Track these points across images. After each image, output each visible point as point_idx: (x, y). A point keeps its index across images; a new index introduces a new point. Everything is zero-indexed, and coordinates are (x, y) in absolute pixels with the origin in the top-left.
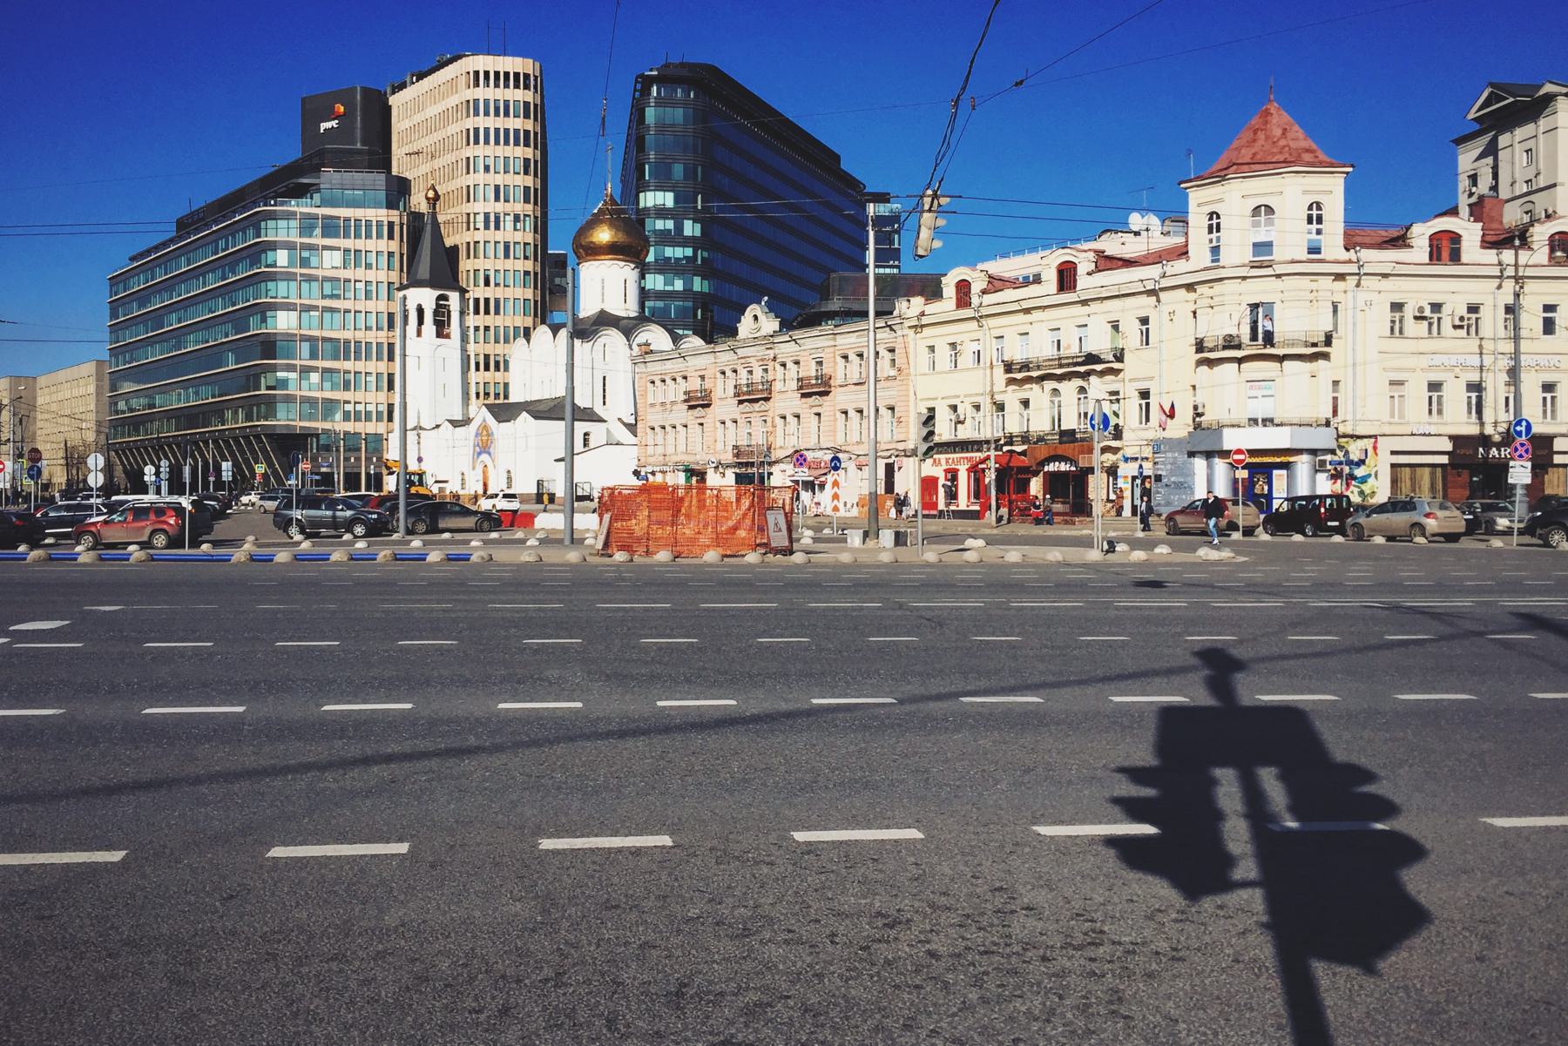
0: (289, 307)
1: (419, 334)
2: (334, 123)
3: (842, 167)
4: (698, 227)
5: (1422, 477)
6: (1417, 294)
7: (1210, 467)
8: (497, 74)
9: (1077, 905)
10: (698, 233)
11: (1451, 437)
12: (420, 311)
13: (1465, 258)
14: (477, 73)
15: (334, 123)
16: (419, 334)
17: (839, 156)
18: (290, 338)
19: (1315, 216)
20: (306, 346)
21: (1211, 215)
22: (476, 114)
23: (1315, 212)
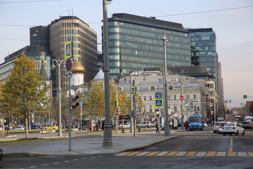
2: (36, 35)
15: (36, 35)
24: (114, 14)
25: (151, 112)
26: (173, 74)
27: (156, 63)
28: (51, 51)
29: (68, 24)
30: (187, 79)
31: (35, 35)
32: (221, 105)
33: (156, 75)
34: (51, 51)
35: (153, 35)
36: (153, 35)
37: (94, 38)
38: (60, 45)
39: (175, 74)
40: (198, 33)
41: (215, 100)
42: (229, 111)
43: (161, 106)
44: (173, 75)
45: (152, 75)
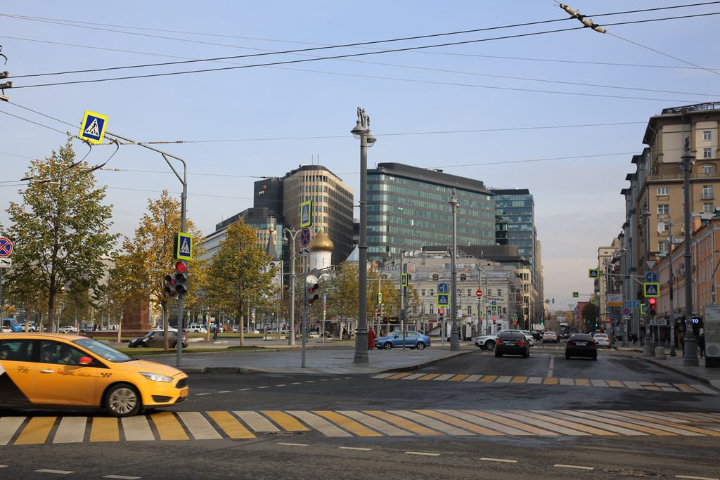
2: (263, 192)
15: (263, 192)
26: (467, 257)
30: (489, 265)
37: (349, 199)
40: (507, 196)
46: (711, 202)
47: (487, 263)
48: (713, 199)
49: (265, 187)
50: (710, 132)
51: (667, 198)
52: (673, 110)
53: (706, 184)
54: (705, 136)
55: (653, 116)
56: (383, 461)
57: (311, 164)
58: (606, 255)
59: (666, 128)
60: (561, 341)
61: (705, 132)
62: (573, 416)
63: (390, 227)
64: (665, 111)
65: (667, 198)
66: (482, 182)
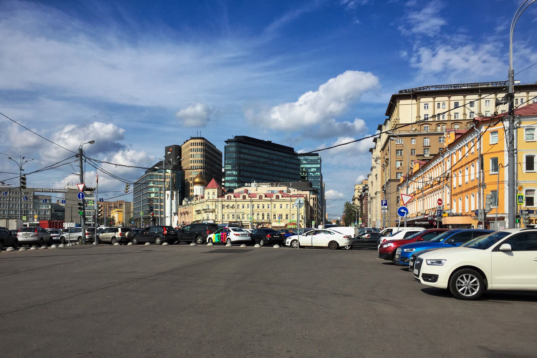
0: (153, 193)
1: (168, 199)
2: (170, 153)
3: (498, 94)
4: (236, 172)
5: (46, 237)
6: (226, 204)
7: (463, 210)
8: (198, 143)
9: (378, 314)
10: (236, 174)
11: (229, 222)
12: (168, 195)
13: (232, 199)
14: (192, 143)
15: (170, 153)
16: (168, 199)
17: (293, 149)
18: (153, 198)
19: (214, 194)
20: (156, 200)
21: (208, 193)
22: (194, 151)
23: (214, 193)
24: (236, 136)
25: (268, 219)
26: (282, 186)
27: (271, 179)
28: (182, 167)
29: (196, 143)
30: (294, 191)
31: (169, 153)
32: (196, 144)
33: (267, 186)
34: (182, 167)
35: (267, 155)
36: (267, 155)
37: (220, 157)
38: (188, 161)
39: (284, 186)
40: (307, 157)
41: (250, 231)
42: (237, 156)
43: (522, 202)
44: (280, 187)
45: (263, 186)
46: (428, 148)
47: (294, 190)
48: (430, 146)
49: (171, 150)
50: (428, 104)
51: (401, 145)
52: (406, 91)
53: (425, 137)
54: (425, 107)
55: (394, 94)
56: (418, 194)
57: (279, 226)
58: (359, 188)
59: (402, 102)
60: (385, 189)
61: (425, 104)
62: (146, 176)
63: (226, 149)
64: (401, 92)
65: (401, 145)
66: (293, 149)
